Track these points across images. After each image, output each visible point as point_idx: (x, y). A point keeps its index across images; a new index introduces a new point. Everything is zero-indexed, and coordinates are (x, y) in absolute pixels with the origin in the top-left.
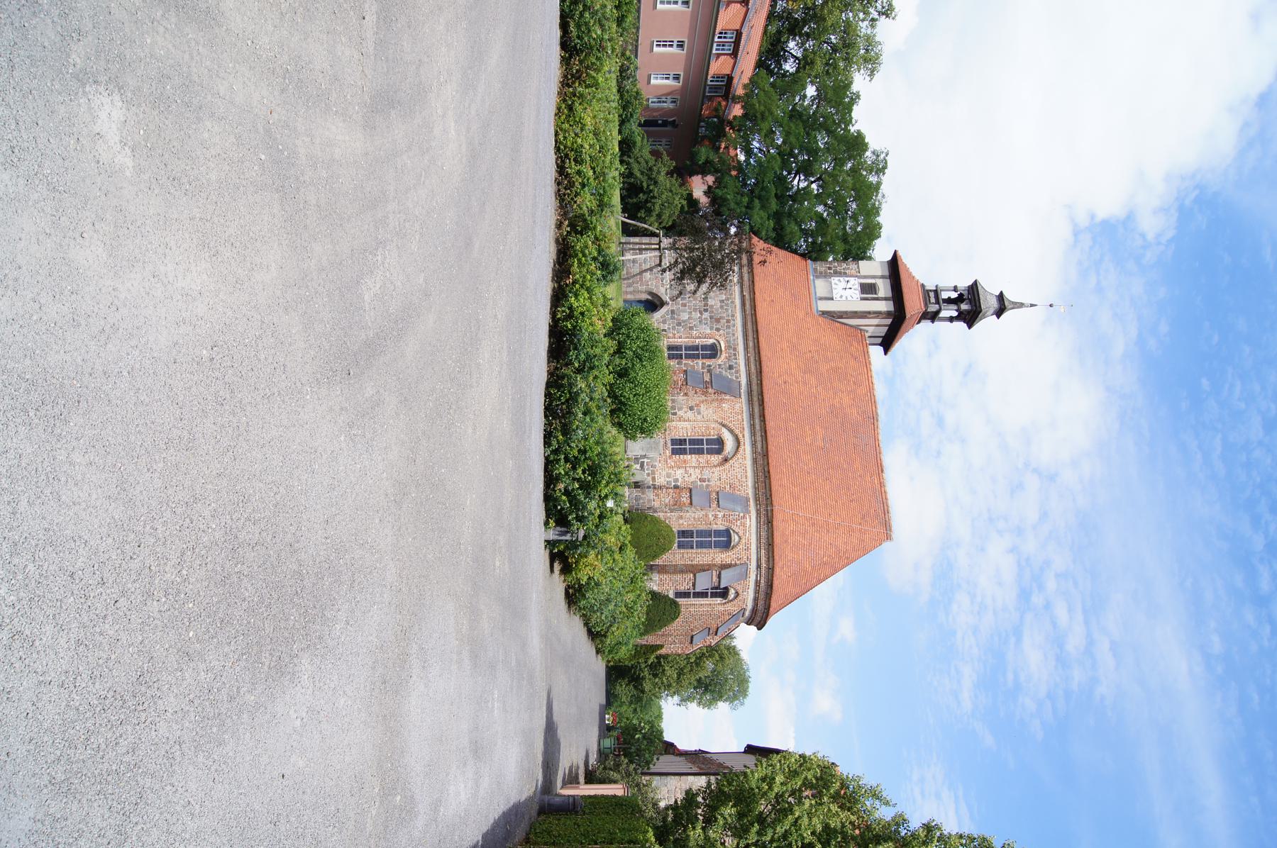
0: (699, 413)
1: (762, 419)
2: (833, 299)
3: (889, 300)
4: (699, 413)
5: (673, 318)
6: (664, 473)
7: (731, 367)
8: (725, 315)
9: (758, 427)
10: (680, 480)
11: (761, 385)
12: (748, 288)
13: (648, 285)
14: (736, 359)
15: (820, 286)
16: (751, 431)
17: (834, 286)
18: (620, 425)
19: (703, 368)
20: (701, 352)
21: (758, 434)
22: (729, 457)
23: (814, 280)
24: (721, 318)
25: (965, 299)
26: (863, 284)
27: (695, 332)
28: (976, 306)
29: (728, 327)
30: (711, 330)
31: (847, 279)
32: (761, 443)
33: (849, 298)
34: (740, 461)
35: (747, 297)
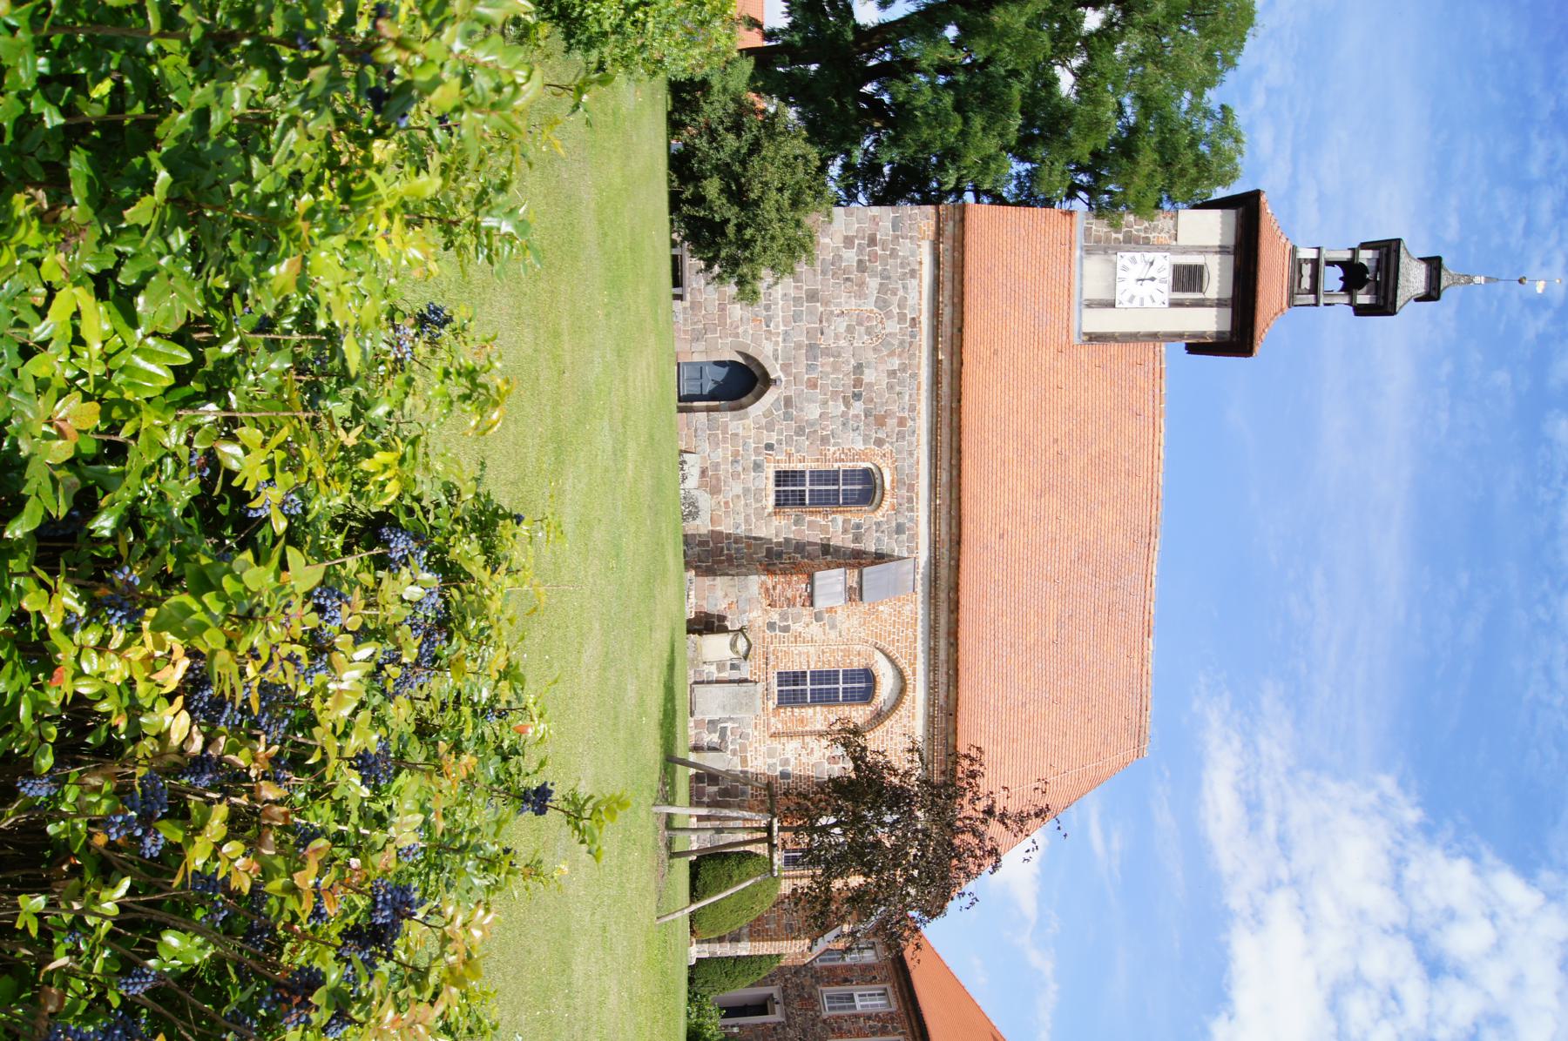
0: (833, 627)
1: (952, 640)
2: (1114, 306)
3: (1226, 305)
4: (833, 627)
5: (787, 417)
6: (763, 749)
7: (900, 529)
8: (895, 408)
9: (942, 655)
10: (793, 761)
11: (956, 568)
12: (949, 342)
13: (737, 335)
14: (912, 511)
15: (1092, 275)
16: (930, 660)
17: (1120, 273)
18: (693, 504)
19: (845, 531)
20: (842, 487)
21: (943, 669)
22: (885, 709)
23: (1081, 258)
24: (887, 414)
25: (1368, 281)
26: (1184, 267)
27: (832, 449)
28: (1385, 298)
29: (900, 436)
30: (865, 443)
31: (1149, 256)
32: (945, 688)
33: (1148, 303)
34: (905, 721)
35: (946, 365)
